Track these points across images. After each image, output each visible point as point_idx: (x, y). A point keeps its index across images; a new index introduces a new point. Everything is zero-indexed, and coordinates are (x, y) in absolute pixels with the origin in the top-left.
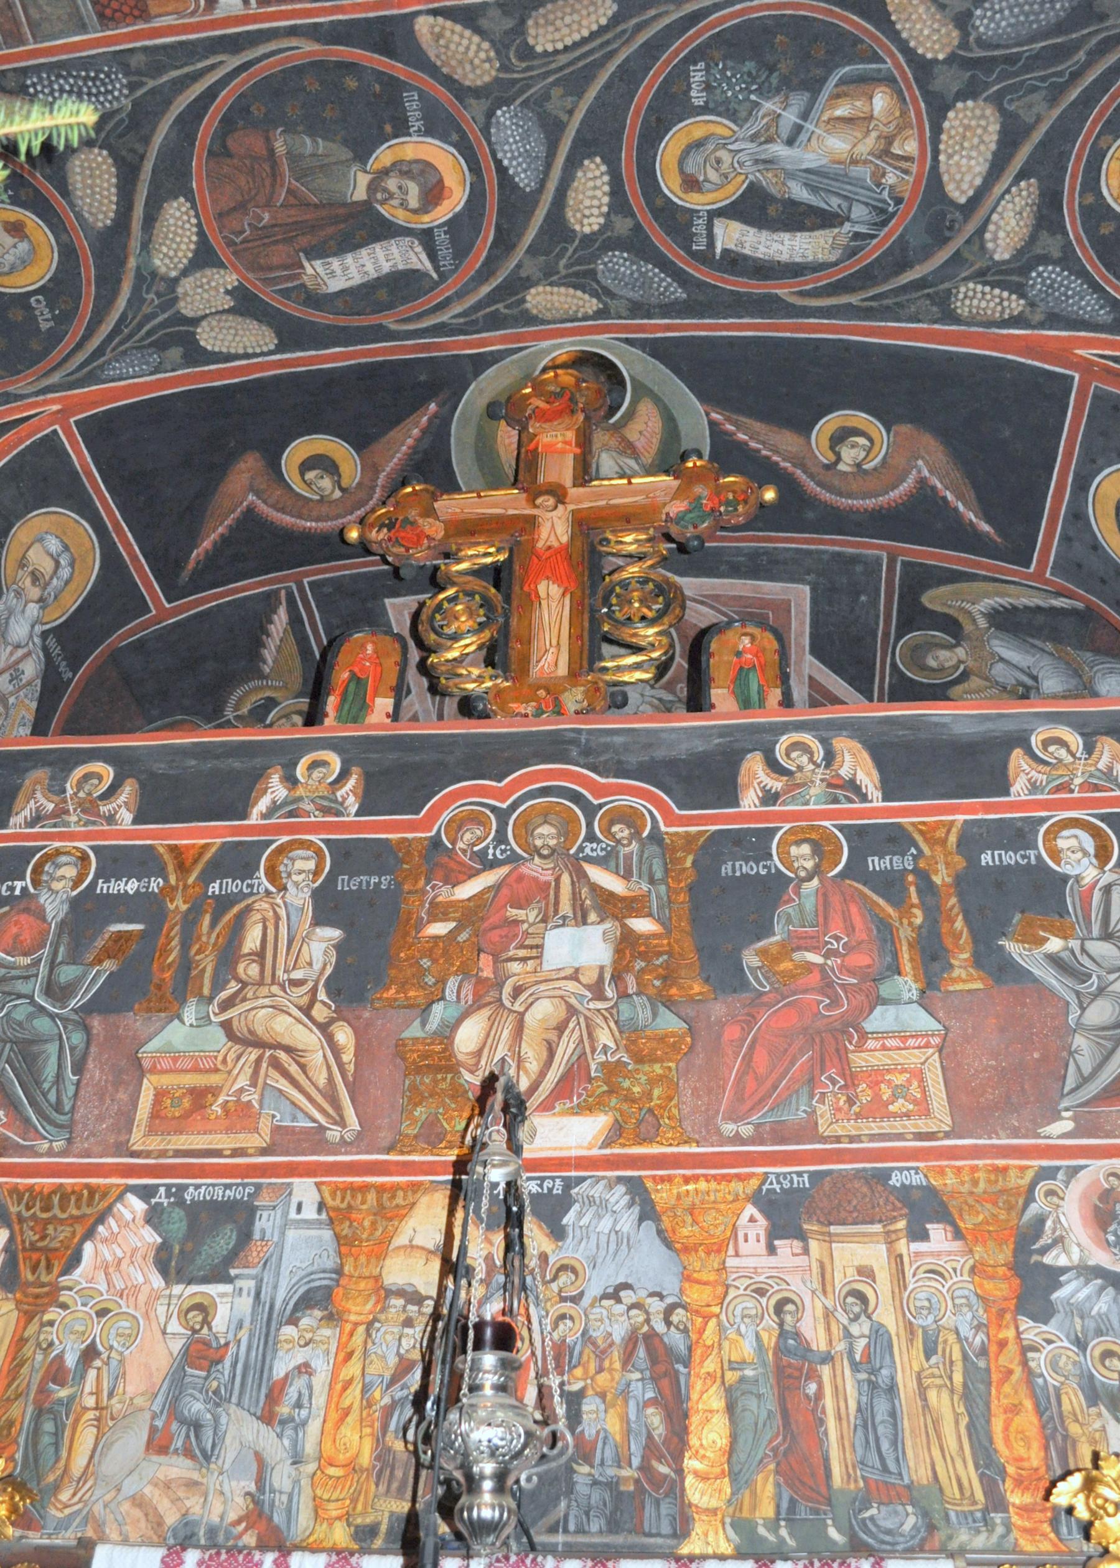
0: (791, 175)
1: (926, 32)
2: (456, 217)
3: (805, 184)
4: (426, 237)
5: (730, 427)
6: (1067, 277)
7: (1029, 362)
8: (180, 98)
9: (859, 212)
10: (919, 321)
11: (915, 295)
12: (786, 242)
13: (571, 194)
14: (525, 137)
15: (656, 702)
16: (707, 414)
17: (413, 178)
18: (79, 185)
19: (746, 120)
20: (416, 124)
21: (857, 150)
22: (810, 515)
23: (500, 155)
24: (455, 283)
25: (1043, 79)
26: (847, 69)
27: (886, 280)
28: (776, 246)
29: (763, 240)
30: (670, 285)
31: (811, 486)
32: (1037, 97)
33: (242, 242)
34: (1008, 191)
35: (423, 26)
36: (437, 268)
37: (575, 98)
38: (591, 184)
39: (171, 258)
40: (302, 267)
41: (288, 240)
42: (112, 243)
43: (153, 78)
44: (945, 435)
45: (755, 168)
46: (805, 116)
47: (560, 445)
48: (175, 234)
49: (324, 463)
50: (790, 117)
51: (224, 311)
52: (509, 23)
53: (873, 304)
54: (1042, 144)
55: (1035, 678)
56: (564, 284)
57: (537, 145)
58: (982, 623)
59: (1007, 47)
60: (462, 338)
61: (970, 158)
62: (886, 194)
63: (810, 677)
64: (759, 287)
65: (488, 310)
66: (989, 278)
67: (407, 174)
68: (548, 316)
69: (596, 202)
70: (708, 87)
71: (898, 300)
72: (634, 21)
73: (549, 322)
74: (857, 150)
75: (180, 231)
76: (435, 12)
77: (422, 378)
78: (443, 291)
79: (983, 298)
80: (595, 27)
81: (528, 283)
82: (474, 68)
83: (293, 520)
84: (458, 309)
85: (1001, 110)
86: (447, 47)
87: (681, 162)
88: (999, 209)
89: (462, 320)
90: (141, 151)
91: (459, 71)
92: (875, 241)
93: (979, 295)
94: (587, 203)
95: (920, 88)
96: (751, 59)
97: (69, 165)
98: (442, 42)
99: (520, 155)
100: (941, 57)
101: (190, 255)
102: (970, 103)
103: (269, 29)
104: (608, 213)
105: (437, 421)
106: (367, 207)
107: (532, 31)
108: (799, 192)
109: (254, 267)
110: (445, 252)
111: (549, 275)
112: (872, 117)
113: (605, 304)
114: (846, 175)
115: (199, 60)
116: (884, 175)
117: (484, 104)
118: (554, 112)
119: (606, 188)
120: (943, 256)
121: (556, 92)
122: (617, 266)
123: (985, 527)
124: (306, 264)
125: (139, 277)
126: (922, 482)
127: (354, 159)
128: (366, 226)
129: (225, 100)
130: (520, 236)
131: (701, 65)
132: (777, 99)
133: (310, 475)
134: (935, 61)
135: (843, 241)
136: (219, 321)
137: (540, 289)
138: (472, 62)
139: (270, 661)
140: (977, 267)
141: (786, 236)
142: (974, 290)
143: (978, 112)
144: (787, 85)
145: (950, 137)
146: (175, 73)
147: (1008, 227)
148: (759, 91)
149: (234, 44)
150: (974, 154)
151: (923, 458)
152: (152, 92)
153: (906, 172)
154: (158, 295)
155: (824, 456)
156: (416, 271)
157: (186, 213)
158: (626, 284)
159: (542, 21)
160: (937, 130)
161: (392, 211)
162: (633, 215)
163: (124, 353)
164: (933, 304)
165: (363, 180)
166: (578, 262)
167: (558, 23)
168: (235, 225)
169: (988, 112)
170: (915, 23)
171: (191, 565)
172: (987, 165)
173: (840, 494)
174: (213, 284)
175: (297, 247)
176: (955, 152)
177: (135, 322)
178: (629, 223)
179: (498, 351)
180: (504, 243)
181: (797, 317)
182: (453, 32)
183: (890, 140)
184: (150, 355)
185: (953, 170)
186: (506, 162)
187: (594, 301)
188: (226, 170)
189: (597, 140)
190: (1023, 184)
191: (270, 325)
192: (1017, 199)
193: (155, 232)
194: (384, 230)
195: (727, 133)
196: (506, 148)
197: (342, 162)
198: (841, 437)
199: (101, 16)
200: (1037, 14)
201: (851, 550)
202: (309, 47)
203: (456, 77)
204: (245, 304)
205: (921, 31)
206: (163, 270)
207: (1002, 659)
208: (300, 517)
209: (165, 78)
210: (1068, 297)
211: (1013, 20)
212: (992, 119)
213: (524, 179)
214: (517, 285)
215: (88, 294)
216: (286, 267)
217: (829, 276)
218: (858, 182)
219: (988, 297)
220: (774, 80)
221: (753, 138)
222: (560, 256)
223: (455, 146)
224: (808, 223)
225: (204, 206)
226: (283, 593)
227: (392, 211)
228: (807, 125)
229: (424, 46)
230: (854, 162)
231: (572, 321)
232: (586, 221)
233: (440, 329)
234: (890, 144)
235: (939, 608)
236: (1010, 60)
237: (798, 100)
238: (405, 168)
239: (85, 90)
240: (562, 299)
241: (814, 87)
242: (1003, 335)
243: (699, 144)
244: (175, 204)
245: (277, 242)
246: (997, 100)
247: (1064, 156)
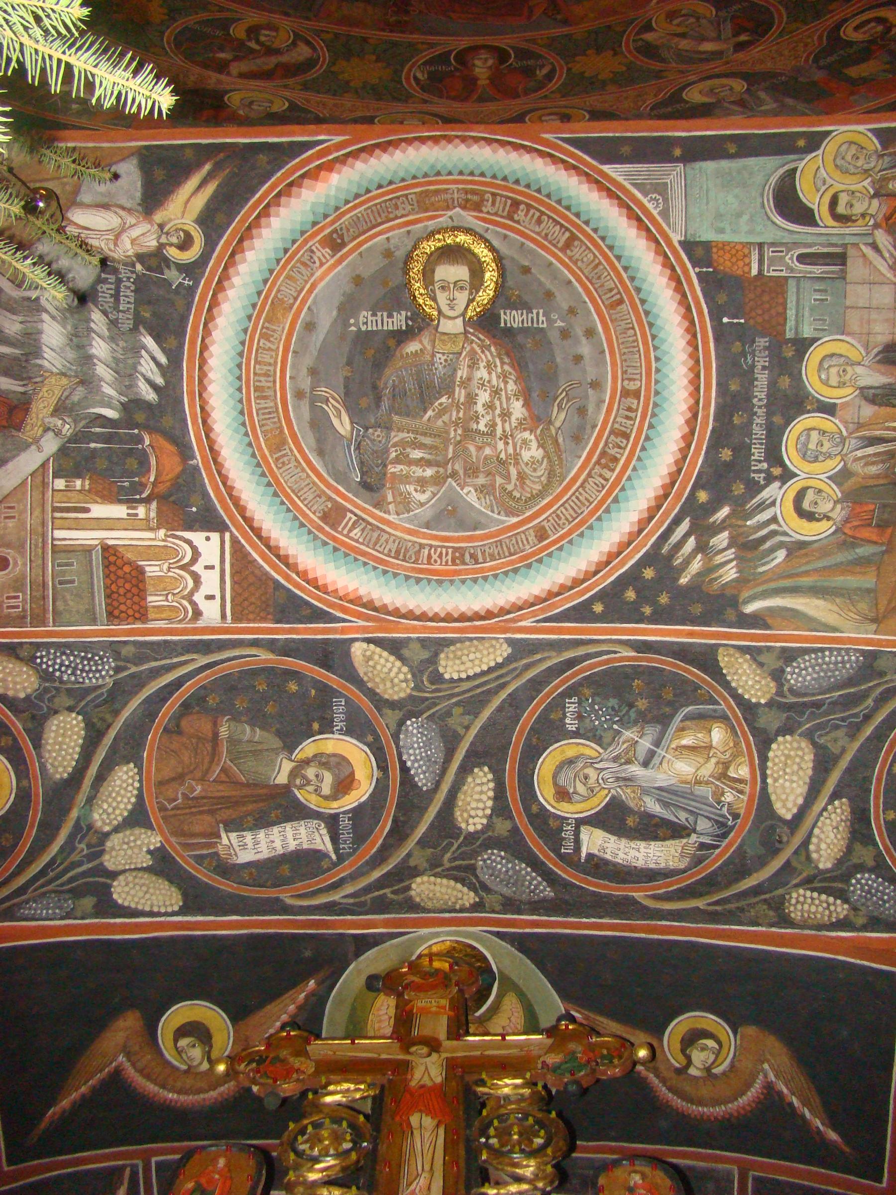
0: (646, 791)
1: (750, 683)
2: (361, 806)
3: (658, 800)
4: (332, 822)
6: (882, 884)
7: (858, 962)
8: (153, 683)
9: (703, 825)
10: (758, 925)
11: (753, 900)
12: (642, 850)
13: (461, 796)
14: (428, 744)
17: (329, 769)
18: (51, 741)
19: (610, 745)
20: (339, 725)
21: (700, 773)
22: (663, 1124)
23: (404, 757)
24: (350, 866)
25: (843, 719)
26: (690, 708)
27: (729, 885)
28: (633, 853)
29: (622, 847)
30: (539, 883)
31: (663, 1091)
32: (840, 733)
33: (172, 809)
34: (825, 809)
35: (358, 650)
36: (336, 850)
37: (472, 717)
38: (478, 789)
39: (108, 814)
40: (219, 837)
41: (211, 812)
42: (63, 792)
43: (136, 665)
44: (789, 1039)
45: (616, 784)
46: (657, 743)
47: (434, 1009)
48: (118, 793)
49: (198, 1031)
50: (645, 744)
51: (142, 869)
52: (425, 655)
53: (718, 908)
54: (848, 770)
56: (446, 877)
57: (437, 752)
59: (814, 695)
60: (349, 917)
61: (792, 781)
62: (725, 809)
64: (618, 889)
65: (377, 893)
66: (817, 885)
67: (325, 765)
68: (429, 905)
69: (481, 805)
70: (580, 717)
71: (739, 904)
72: (525, 661)
73: (429, 911)
74: (700, 773)
75: (122, 792)
76: (369, 641)
77: (308, 954)
78: (339, 872)
79: (812, 903)
80: (492, 664)
81: (415, 872)
82: (393, 686)
83: (156, 1088)
84: (349, 889)
85: (814, 744)
86: (374, 667)
87: (555, 776)
88: (819, 824)
89: (351, 901)
90: (110, 721)
91: (381, 686)
92: (717, 851)
93: (809, 901)
94: (474, 805)
95: (748, 725)
96: (614, 697)
97: (48, 723)
98: (371, 663)
99: (422, 758)
100: (763, 701)
101: (126, 814)
102: (788, 737)
103: (236, 640)
104: (491, 816)
105: (314, 998)
106: (286, 789)
107: (443, 663)
108: (653, 807)
109: (179, 833)
110: (346, 835)
111: (434, 867)
112: (711, 747)
113: (481, 898)
114: (692, 793)
115: (176, 656)
116: (723, 794)
117: (398, 714)
118: (453, 727)
119: (491, 794)
120: (776, 864)
121: (457, 711)
122: (495, 864)
123: (833, 1135)
124: (223, 835)
125: (77, 826)
126: (769, 1087)
127: (283, 749)
128: (283, 806)
129: (187, 690)
130: (414, 828)
131: (575, 699)
132: (635, 729)
133: (183, 1042)
134: (758, 704)
135: (691, 850)
136: (136, 877)
137: (425, 878)
138: (392, 681)
140: (805, 875)
141: (642, 845)
142: (804, 896)
143: (795, 745)
144: (644, 719)
145: (775, 764)
146: (154, 664)
147: (828, 840)
148: (621, 722)
149: (206, 647)
150: (795, 778)
151: (768, 1061)
152: (132, 676)
153: (741, 792)
154: (89, 846)
155: (677, 1061)
156: (319, 851)
157: (132, 777)
158: (502, 881)
159: (451, 656)
160: (764, 759)
161: (308, 796)
162: (511, 818)
163: (44, 894)
164: (770, 907)
165: (287, 766)
166: (462, 857)
167: (464, 658)
168: (170, 794)
169: (803, 745)
170: (741, 676)
171: (44, 1124)
172: (806, 787)
173: (691, 1101)
174: (139, 843)
175: (219, 818)
176: (780, 776)
177: (62, 867)
178: (508, 825)
179: (380, 934)
180: (399, 833)
181: (652, 919)
182: (380, 656)
183: (726, 765)
184: (66, 900)
185: (779, 791)
186: (409, 764)
187: (472, 894)
188: (175, 746)
189: (487, 753)
190: (836, 802)
191: (179, 887)
192: (833, 816)
193: (101, 790)
194: (296, 812)
195: (594, 754)
196: (411, 751)
197: (273, 750)
198: (692, 1038)
199: (110, 614)
200: (833, 671)
201: (702, 1164)
202: (265, 656)
203: (378, 691)
204: (163, 865)
205: (746, 682)
206: (99, 824)
208: (163, 1086)
209: (145, 667)
210: (885, 902)
211: (815, 676)
212: (806, 750)
213: (422, 780)
214: (405, 873)
215: (29, 835)
216: (204, 835)
217: (676, 882)
218: (703, 800)
219: (817, 902)
220: (633, 714)
221: (615, 759)
222: (445, 850)
223: (368, 745)
224: (660, 833)
225: (149, 772)
226: (128, 1171)
227: (308, 796)
228: (659, 751)
229: (356, 665)
230: (698, 782)
231: (450, 912)
232: (471, 821)
233: (329, 908)
234: (727, 768)
236: (817, 705)
237: (652, 731)
238: (323, 760)
239: (80, 666)
240: (444, 890)
241: (664, 721)
242: (832, 938)
243: (571, 762)
244: (125, 769)
245: (201, 813)
246: (809, 735)
247: (868, 780)
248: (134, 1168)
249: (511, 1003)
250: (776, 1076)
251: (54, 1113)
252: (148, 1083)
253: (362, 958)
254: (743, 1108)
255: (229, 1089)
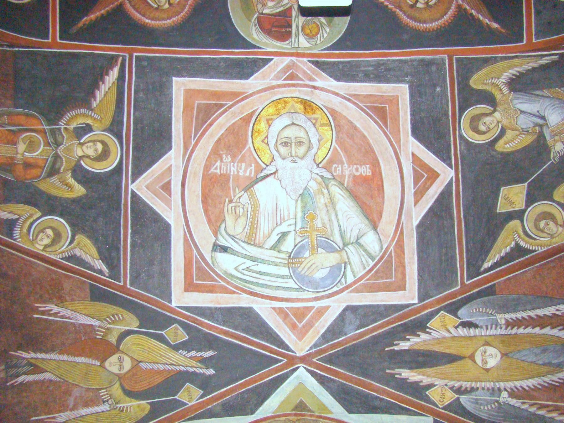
15: (319, 179)
31: (405, 19)
55: (543, 118)
58: (506, 90)
63: (413, 154)
83: (140, 16)
123: (495, 25)
139: (98, 99)
171: (81, 24)
207: (522, 112)
208: (144, 16)
226: (121, 58)
235: (480, 87)
248: (124, 57)
251: (86, 20)
252: (136, 13)
254: (447, 21)
255: (178, 19)
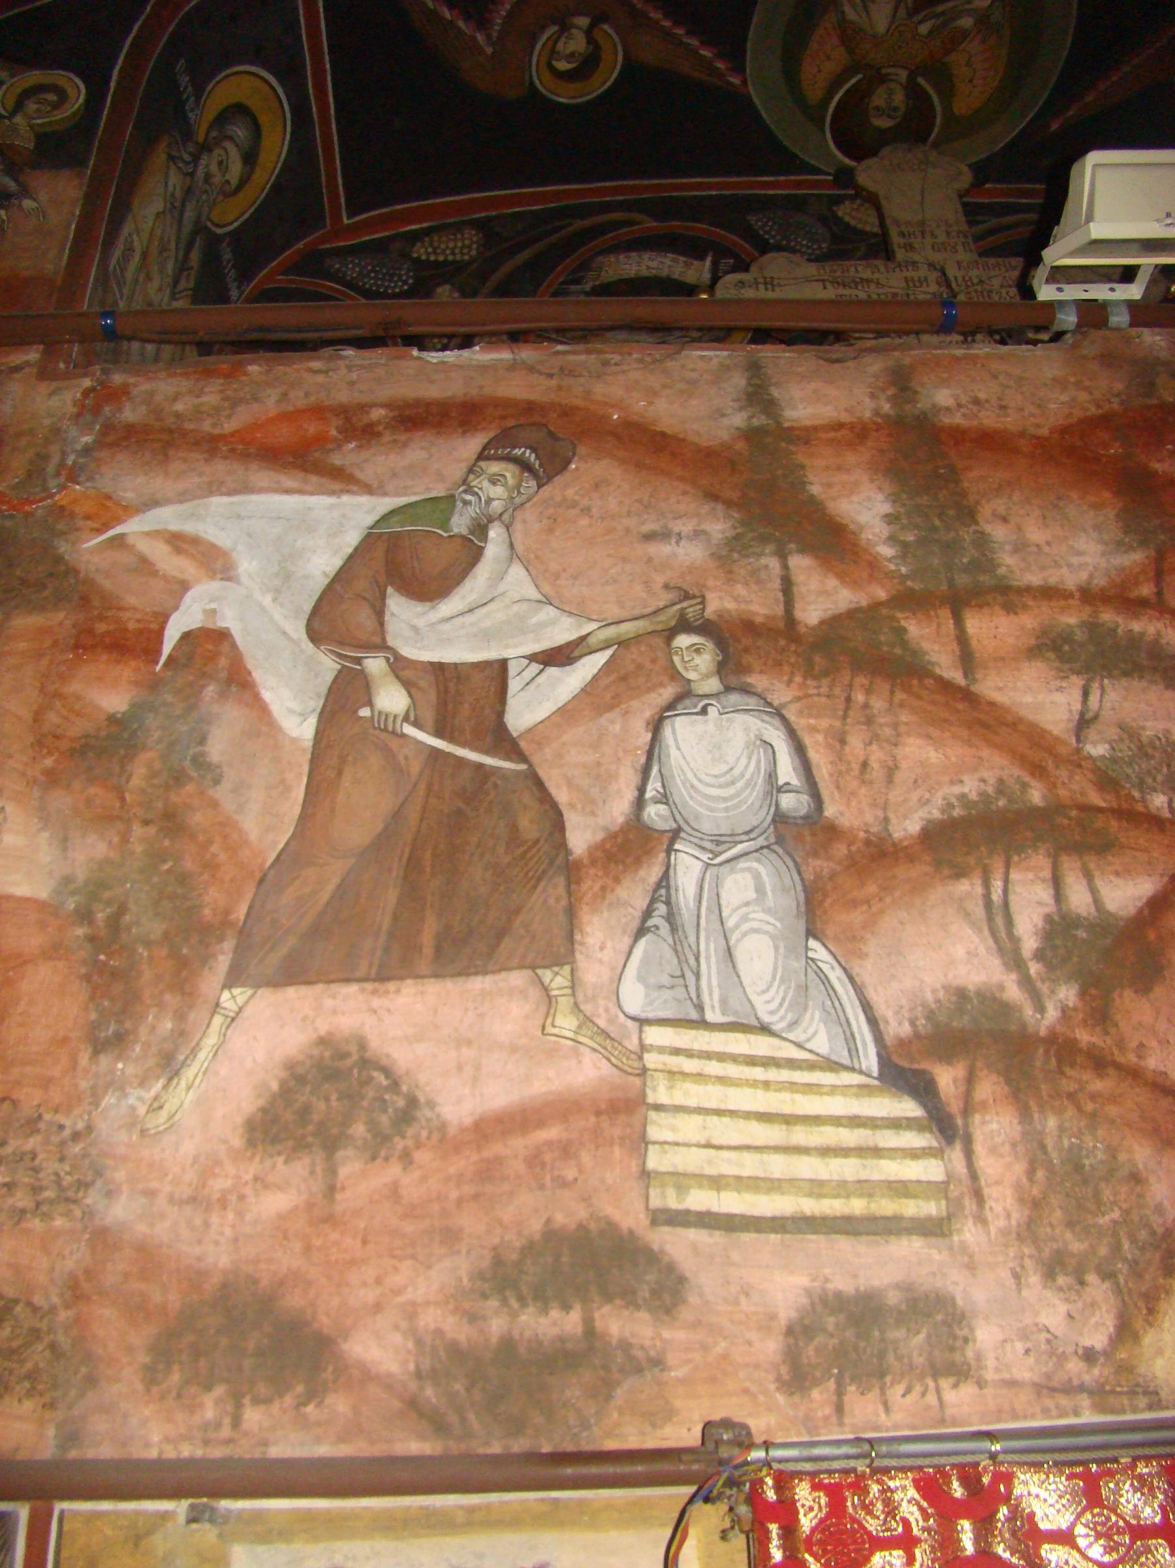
5: (720, 65)
16: (744, 82)
28: (654, 264)
53: (557, 224)
126: (483, 23)
141: (645, 273)
187: (840, 214)
198: (587, 65)
210: (373, 271)
249: (814, 91)
250: (474, 39)
253: (983, 156)
